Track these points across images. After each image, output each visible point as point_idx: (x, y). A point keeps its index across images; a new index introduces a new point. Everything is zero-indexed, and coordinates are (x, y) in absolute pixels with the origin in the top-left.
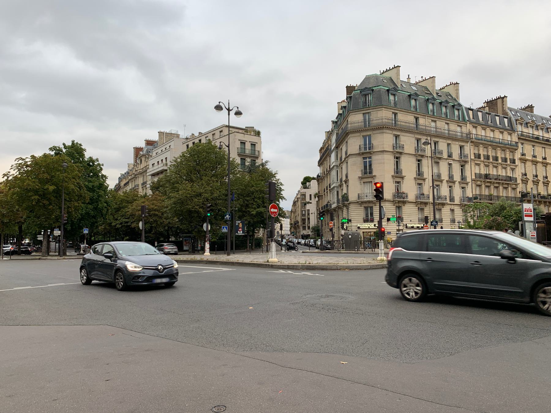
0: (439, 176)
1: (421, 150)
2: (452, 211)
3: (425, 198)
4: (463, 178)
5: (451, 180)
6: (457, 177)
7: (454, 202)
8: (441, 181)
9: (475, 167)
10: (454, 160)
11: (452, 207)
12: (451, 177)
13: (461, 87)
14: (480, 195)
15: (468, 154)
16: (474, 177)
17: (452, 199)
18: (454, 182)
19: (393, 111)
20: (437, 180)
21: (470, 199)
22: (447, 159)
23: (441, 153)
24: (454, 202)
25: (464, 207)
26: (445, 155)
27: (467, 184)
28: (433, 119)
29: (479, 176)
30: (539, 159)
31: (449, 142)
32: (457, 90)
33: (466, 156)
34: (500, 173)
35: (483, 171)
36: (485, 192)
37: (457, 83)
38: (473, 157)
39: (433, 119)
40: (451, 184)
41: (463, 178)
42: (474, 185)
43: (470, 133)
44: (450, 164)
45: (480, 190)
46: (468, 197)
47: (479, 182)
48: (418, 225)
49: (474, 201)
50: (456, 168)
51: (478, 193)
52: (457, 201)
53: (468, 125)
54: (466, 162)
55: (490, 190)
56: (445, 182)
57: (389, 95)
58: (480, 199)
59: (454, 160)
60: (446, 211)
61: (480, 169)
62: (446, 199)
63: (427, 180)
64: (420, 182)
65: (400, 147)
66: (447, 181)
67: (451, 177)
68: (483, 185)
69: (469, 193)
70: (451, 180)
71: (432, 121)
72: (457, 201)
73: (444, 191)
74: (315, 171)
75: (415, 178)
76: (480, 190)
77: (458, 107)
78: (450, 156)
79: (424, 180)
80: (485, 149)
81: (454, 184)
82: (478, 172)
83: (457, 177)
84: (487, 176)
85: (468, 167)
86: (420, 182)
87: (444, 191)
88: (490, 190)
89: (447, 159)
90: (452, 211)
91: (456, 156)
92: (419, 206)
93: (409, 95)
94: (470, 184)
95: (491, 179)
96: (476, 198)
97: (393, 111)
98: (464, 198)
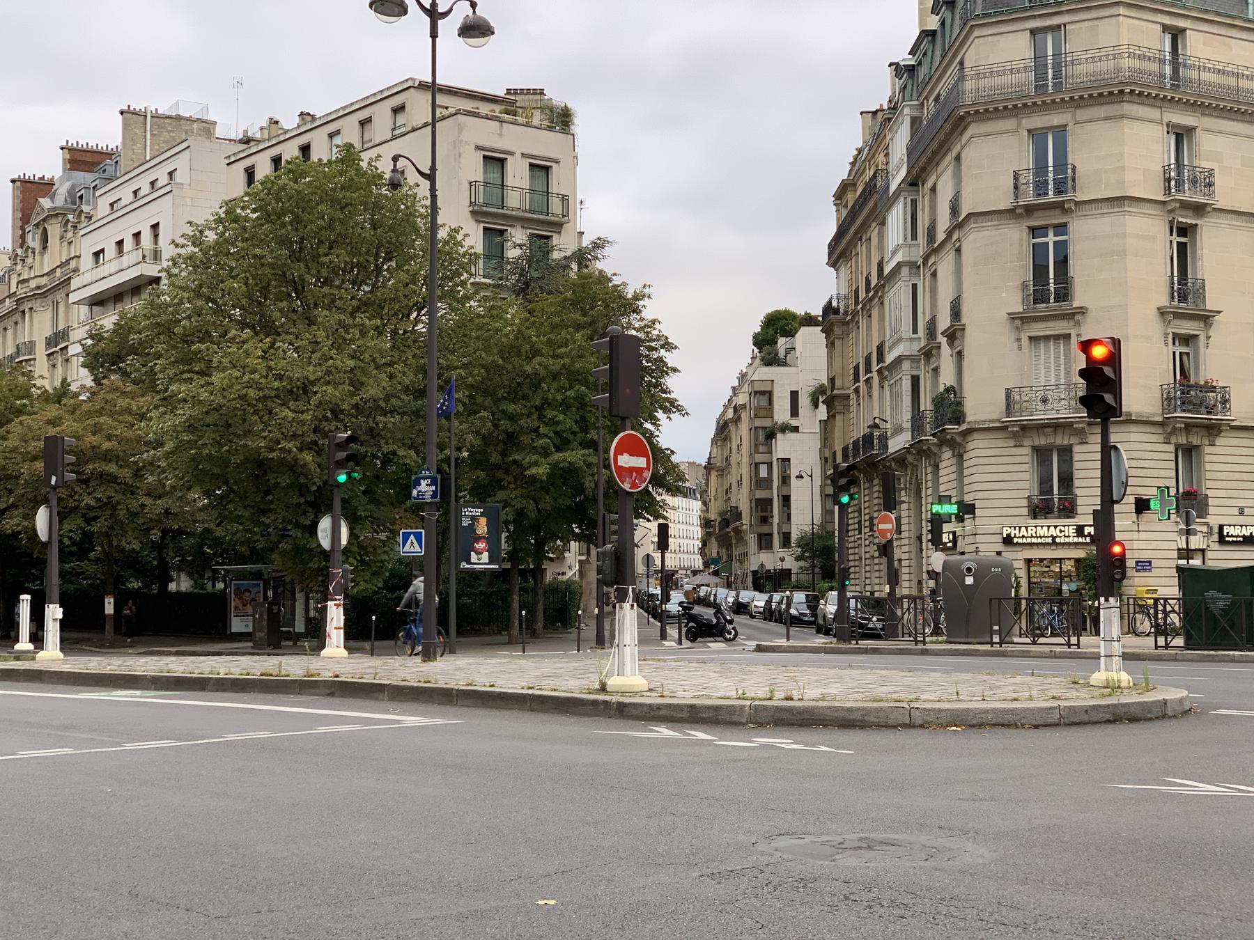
19: (1167, 20)
64: (1186, 327)
79: (1206, 319)
86: (1186, 327)
97: (1167, 20)
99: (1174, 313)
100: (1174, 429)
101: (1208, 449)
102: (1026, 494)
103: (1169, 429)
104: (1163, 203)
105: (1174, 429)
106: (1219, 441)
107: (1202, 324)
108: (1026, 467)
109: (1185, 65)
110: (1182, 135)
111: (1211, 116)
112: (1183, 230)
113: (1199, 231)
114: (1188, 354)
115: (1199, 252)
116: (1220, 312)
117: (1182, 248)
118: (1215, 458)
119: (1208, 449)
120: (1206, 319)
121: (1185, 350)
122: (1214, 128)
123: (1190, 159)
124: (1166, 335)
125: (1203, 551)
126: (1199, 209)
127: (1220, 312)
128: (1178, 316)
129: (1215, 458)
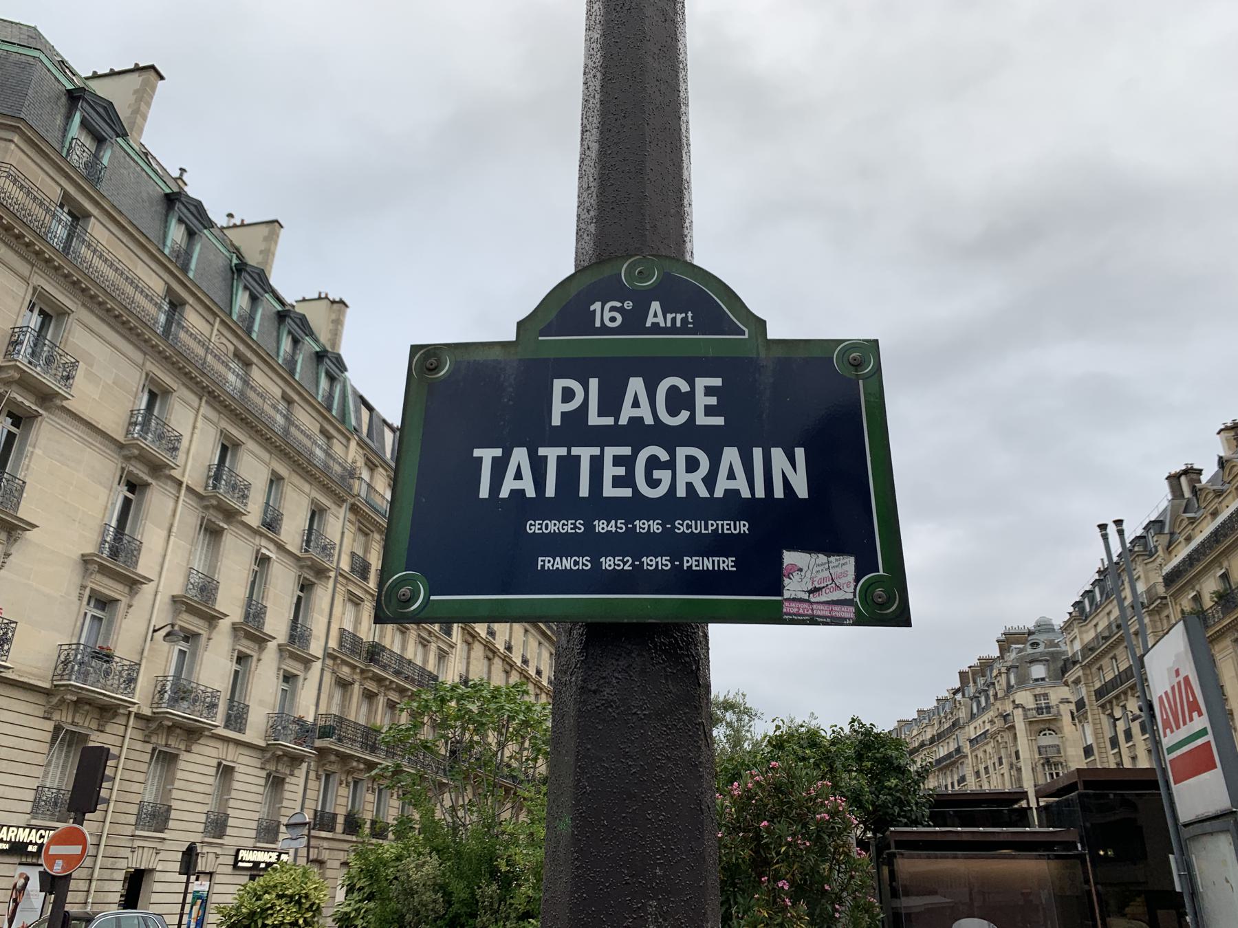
0: (208, 589)
1: (160, 437)
2: (225, 772)
3: (113, 681)
4: (298, 633)
5: (251, 630)
6: (277, 624)
7: (241, 730)
8: (212, 619)
9: (344, 606)
10: (281, 547)
11: (231, 755)
12: (255, 612)
13: (350, 317)
14: (341, 720)
15: (179, 438)
16: (333, 644)
17: (237, 718)
18: (261, 641)
19: (71, 190)
20: (197, 604)
21: (305, 732)
22: (255, 532)
23: (242, 491)
24: (241, 730)
25: (278, 763)
26: (254, 517)
27: (307, 662)
28: (242, 348)
29: (350, 642)
30: (500, 646)
31: (283, 470)
32: (338, 323)
33: (326, 549)
34: (409, 655)
35: (368, 632)
36: (358, 713)
37: (342, 302)
38: (345, 565)
39: (242, 348)
40: (247, 647)
41: (298, 633)
42: (328, 677)
43: (352, 474)
44: (262, 561)
45: (345, 703)
46: (300, 721)
47: (346, 670)
48: (23, 835)
49: (319, 743)
50: (283, 580)
51: (335, 710)
52: (255, 732)
53: (353, 444)
54: (321, 572)
55: (371, 711)
56: (224, 625)
57: (69, 117)
58: (340, 740)
59: (281, 547)
60: (197, 766)
61: (357, 622)
62: (213, 706)
63: (148, 589)
64: (110, 588)
65: (49, 361)
66: (235, 628)
67: (255, 612)
68: (356, 686)
69: (307, 707)
70: (251, 630)
71: (237, 355)
72: (255, 732)
73: (214, 668)
74: (957, 685)
75: (86, 560)
76: (345, 703)
77: (334, 370)
78: (271, 524)
79: (133, 584)
80: (361, 538)
81: (262, 649)
82: (349, 627)
83: (277, 624)
84: (374, 653)
85: (322, 595)
86: (110, 588)
87: (214, 668)
88: (371, 711)
89: (255, 532)
90: (225, 772)
91: (292, 530)
92: (64, 717)
93: (167, 195)
94: (317, 666)
95: (384, 667)
96: (326, 732)
97: (71, 190)
98: (282, 721)
99: (100, 565)
100: (63, 701)
101: (184, 756)
102: (206, 809)
103: (55, 700)
104: (297, 558)
105: (63, 701)
106: (195, 748)
107: (127, 590)
108: (259, 798)
109: (179, 324)
110: (156, 395)
111: (92, 311)
112: (132, 487)
113: (36, 425)
114: (100, 619)
115: (29, 448)
116: (34, 526)
117: (127, 503)
118: (191, 767)
119: (184, 756)
120: (133, 584)
121: (98, 613)
122: (93, 327)
123: (159, 412)
124: (83, 587)
125: (211, 874)
126: (46, 398)
127: (34, 526)
128: (103, 570)
129: (191, 767)
